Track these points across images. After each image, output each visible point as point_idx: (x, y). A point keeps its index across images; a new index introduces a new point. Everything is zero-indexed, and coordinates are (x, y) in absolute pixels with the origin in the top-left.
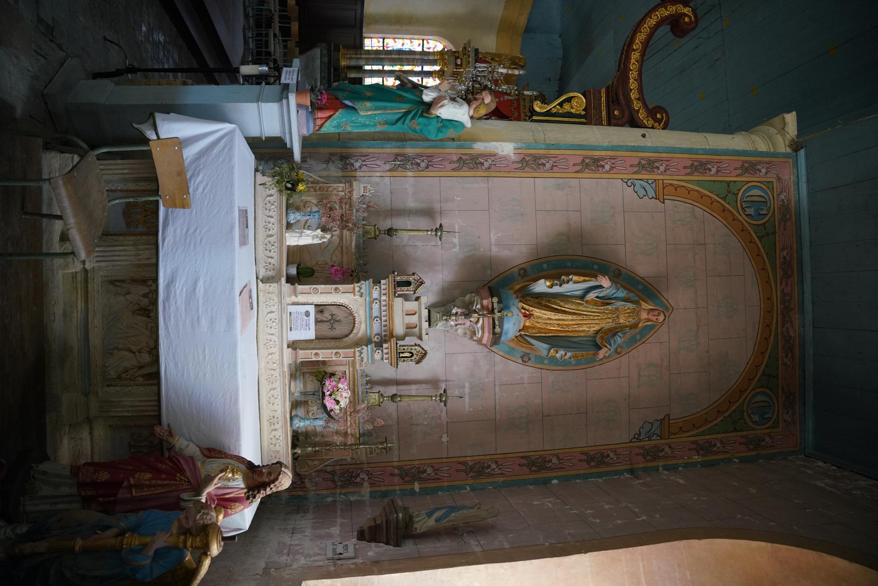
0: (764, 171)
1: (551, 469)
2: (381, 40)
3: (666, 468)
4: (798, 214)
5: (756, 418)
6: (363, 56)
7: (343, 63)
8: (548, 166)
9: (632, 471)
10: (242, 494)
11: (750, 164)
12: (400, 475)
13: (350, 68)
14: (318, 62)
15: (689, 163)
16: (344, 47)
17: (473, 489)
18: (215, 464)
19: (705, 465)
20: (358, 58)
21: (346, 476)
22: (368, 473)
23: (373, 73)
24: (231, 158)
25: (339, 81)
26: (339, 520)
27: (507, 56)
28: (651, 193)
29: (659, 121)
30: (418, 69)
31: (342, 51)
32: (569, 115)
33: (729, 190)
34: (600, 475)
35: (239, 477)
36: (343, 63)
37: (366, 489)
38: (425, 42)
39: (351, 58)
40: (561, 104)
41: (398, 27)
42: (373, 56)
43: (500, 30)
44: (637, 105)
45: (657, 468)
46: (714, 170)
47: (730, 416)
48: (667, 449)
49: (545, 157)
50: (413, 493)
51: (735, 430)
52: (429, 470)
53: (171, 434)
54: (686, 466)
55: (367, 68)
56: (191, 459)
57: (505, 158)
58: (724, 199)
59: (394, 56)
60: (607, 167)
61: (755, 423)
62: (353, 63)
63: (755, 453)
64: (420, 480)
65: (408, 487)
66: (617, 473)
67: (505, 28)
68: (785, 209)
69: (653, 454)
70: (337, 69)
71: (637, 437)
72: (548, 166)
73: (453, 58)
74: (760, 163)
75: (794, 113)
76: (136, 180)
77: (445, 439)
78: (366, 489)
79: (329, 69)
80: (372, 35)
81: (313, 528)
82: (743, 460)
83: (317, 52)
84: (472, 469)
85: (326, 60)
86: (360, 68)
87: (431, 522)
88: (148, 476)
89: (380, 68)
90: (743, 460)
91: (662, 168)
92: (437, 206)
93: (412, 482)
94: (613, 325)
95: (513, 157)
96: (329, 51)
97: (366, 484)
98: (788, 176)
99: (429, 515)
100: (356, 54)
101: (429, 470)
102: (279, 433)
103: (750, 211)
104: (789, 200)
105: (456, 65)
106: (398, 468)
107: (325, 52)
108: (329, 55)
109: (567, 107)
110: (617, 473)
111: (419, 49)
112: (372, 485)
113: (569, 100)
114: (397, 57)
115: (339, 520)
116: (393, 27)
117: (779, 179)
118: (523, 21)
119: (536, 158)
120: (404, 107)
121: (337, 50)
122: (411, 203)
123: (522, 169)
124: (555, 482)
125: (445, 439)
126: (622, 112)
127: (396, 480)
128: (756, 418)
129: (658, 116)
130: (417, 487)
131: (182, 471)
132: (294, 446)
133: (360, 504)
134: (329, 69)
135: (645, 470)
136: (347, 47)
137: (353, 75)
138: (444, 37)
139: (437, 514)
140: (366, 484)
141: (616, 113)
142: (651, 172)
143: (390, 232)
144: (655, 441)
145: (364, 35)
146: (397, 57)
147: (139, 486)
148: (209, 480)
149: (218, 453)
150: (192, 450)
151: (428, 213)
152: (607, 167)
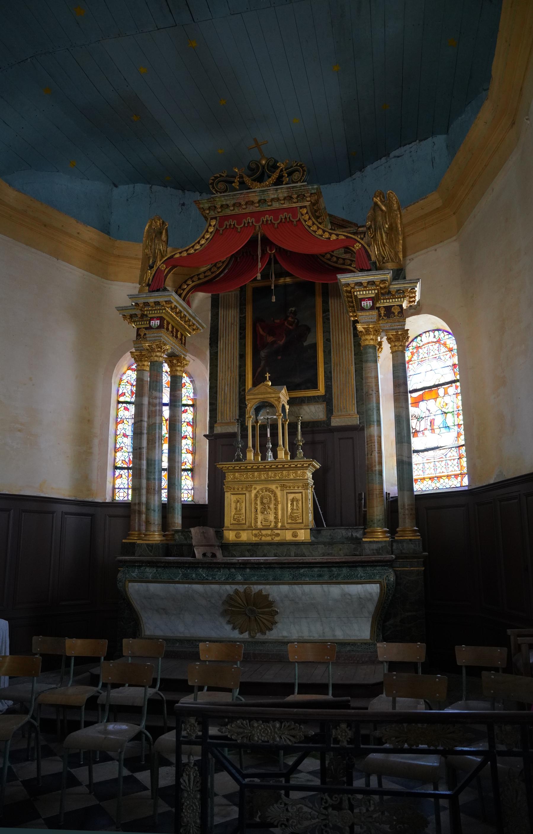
2: (118, 472)
6: (144, 499)
7: (156, 537)
13: (165, 524)
14: (154, 588)
16: (127, 536)
20: (148, 509)
23: (174, 485)
25: (191, 546)
27: (146, 247)
30: (166, 412)
31: (134, 539)
36: (156, 537)
38: (122, 399)
39: (148, 523)
41: (96, 441)
42: (144, 482)
43: (105, 275)
55: (164, 494)
59: (145, 444)
62: (156, 518)
67: (101, 264)
70: (167, 549)
73: (150, 335)
75: (159, 787)
76: (69, 496)
79: (168, 565)
80: (109, 486)
83: (135, 589)
85: (150, 572)
86: (166, 509)
89: (164, 474)
94: (254, 539)
96: (132, 564)
100: (140, 513)
105: (161, 327)
107: (135, 573)
108: (141, 564)
111: (132, 408)
114: (145, 437)
116: (96, 450)
118: (90, 234)
121: (130, 548)
134: (168, 565)
136: (128, 529)
137: (178, 520)
138: (114, 366)
145: (108, 500)
146: (145, 437)
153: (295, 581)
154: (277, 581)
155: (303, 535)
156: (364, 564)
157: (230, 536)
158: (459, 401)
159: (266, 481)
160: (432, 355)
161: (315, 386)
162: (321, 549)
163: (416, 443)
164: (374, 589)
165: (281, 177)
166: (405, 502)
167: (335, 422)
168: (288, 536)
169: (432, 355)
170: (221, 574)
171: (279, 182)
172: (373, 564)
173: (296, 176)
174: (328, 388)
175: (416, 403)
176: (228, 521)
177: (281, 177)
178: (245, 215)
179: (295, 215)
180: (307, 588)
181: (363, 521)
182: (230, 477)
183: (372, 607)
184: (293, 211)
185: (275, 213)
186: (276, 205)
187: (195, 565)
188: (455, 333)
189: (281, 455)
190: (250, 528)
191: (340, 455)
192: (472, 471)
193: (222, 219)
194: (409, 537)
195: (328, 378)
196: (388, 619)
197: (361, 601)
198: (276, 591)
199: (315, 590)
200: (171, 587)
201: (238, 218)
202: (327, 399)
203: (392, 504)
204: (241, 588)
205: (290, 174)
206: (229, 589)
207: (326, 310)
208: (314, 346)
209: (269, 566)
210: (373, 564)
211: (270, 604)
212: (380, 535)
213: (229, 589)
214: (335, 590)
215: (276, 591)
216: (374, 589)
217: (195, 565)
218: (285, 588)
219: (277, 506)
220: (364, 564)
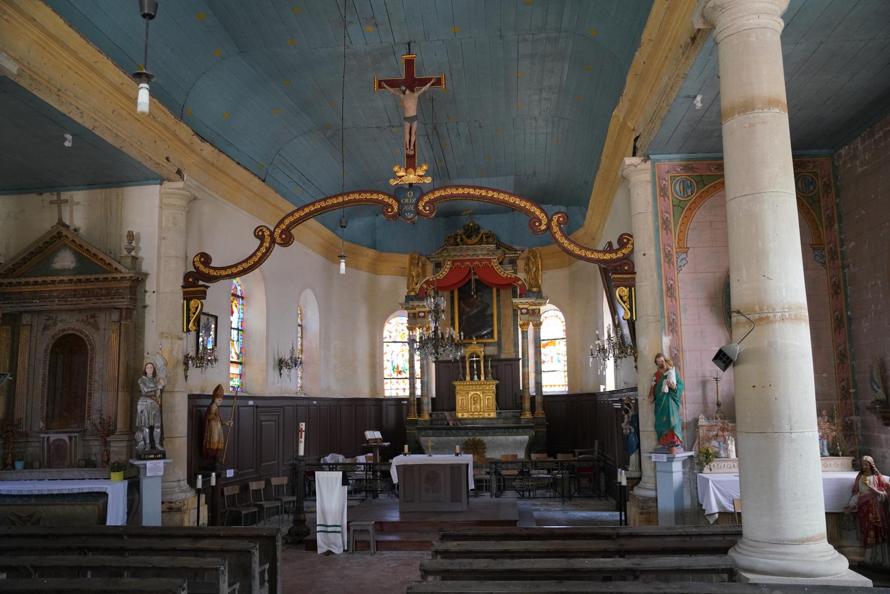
0: (664, 182)
1: (842, 316)
3: (842, 246)
4: (689, 160)
5: (812, 188)
8: (674, 317)
9: (844, 267)
10: (876, 477)
11: (660, 191)
12: (847, 399)
15: (665, 231)
17: (854, 360)
18: (863, 489)
19: (840, 222)
21: (848, 429)
22: (845, 417)
24: (723, 481)
26: (876, 434)
28: (684, 256)
29: (628, 240)
32: (630, 297)
33: (678, 206)
34: (845, 287)
35: (868, 478)
37: (854, 418)
40: (624, 302)
41: (378, 366)
44: (620, 255)
45: (842, 251)
46: (667, 215)
47: (811, 205)
48: (831, 245)
49: (669, 319)
50: (855, 393)
51: (819, 201)
52: (843, 384)
53: (848, 507)
54: (840, 233)
56: (860, 498)
57: (671, 341)
58: (683, 209)
60: (672, 282)
61: (815, 188)
63: (833, 188)
64: (849, 388)
65: (852, 395)
66: (844, 277)
68: (686, 168)
69: (833, 254)
71: (823, 264)
72: (674, 317)
74: (660, 185)
77: (825, 375)
78: (854, 418)
81: (881, 447)
82: (838, 196)
84: (841, 360)
85: (430, 432)
87: (880, 391)
88: (871, 515)
90: (838, 196)
91: (669, 248)
92: (700, 379)
93: (850, 393)
95: (671, 337)
97: (852, 418)
98: (666, 166)
99: (876, 391)
101: (843, 384)
102: (832, 462)
103: (689, 191)
104: (681, 165)
106: (841, 400)
107: (423, 433)
109: (625, 298)
110: (844, 277)
112: (851, 415)
113: (621, 297)
115: (876, 434)
117: (668, 172)
118: (371, 253)
119: (670, 324)
120: (671, 401)
122: (699, 393)
123: (677, 332)
124: (849, 313)
125: (825, 375)
126: (625, 264)
127: (849, 401)
128: (812, 188)
129: (625, 241)
130: (852, 391)
131: (867, 502)
132: (837, 455)
133: (863, 422)
135: (843, 259)
139: (876, 388)
140: (852, 418)
141: (626, 268)
142: (672, 255)
143: (718, 405)
144: (826, 253)
147: (876, 518)
148: (871, 490)
149: (855, 489)
150: (855, 499)
151: (704, 383)
152: (672, 282)
153: (495, 434)
154: (487, 434)
155: (493, 415)
156: (522, 428)
157: (460, 415)
158: (565, 348)
159: (476, 390)
160: (553, 322)
161: (492, 337)
162: (501, 421)
163: (544, 367)
164: (526, 437)
165: (482, 238)
166: (539, 400)
167: (503, 356)
168: (486, 415)
169: (553, 322)
170: (463, 432)
171: (481, 242)
172: (526, 427)
173: (490, 240)
174: (499, 338)
175: (545, 346)
176: (458, 408)
177: (482, 238)
178: (465, 261)
179: (490, 263)
180: (499, 437)
181: (520, 407)
182: (458, 388)
183: (525, 445)
184: (489, 260)
185: (481, 260)
186: (481, 257)
187: (450, 429)
188: (562, 311)
189: (483, 378)
190: (468, 412)
191: (505, 372)
192: (570, 384)
193: (454, 262)
194: (540, 416)
195: (499, 332)
196: (531, 448)
197: (521, 443)
198: (486, 439)
199: (502, 438)
200: (440, 439)
201: (462, 261)
202: (499, 344)
203: (533, 398)
204: (471, 438)
205: (487, 237)
206: (466, 438)
207: (498, 296)
208: (492, 315)
209: (483, 428)
210: (526, 427)
211: (484, 444)
212: (528, 415)
213: (466, 438)
214: (511, 438)
215: (486, 439)
216: (526, 437)
217: (450, 429)
218: (489, 438)
219: (476, 400)
220: (522, 428)
